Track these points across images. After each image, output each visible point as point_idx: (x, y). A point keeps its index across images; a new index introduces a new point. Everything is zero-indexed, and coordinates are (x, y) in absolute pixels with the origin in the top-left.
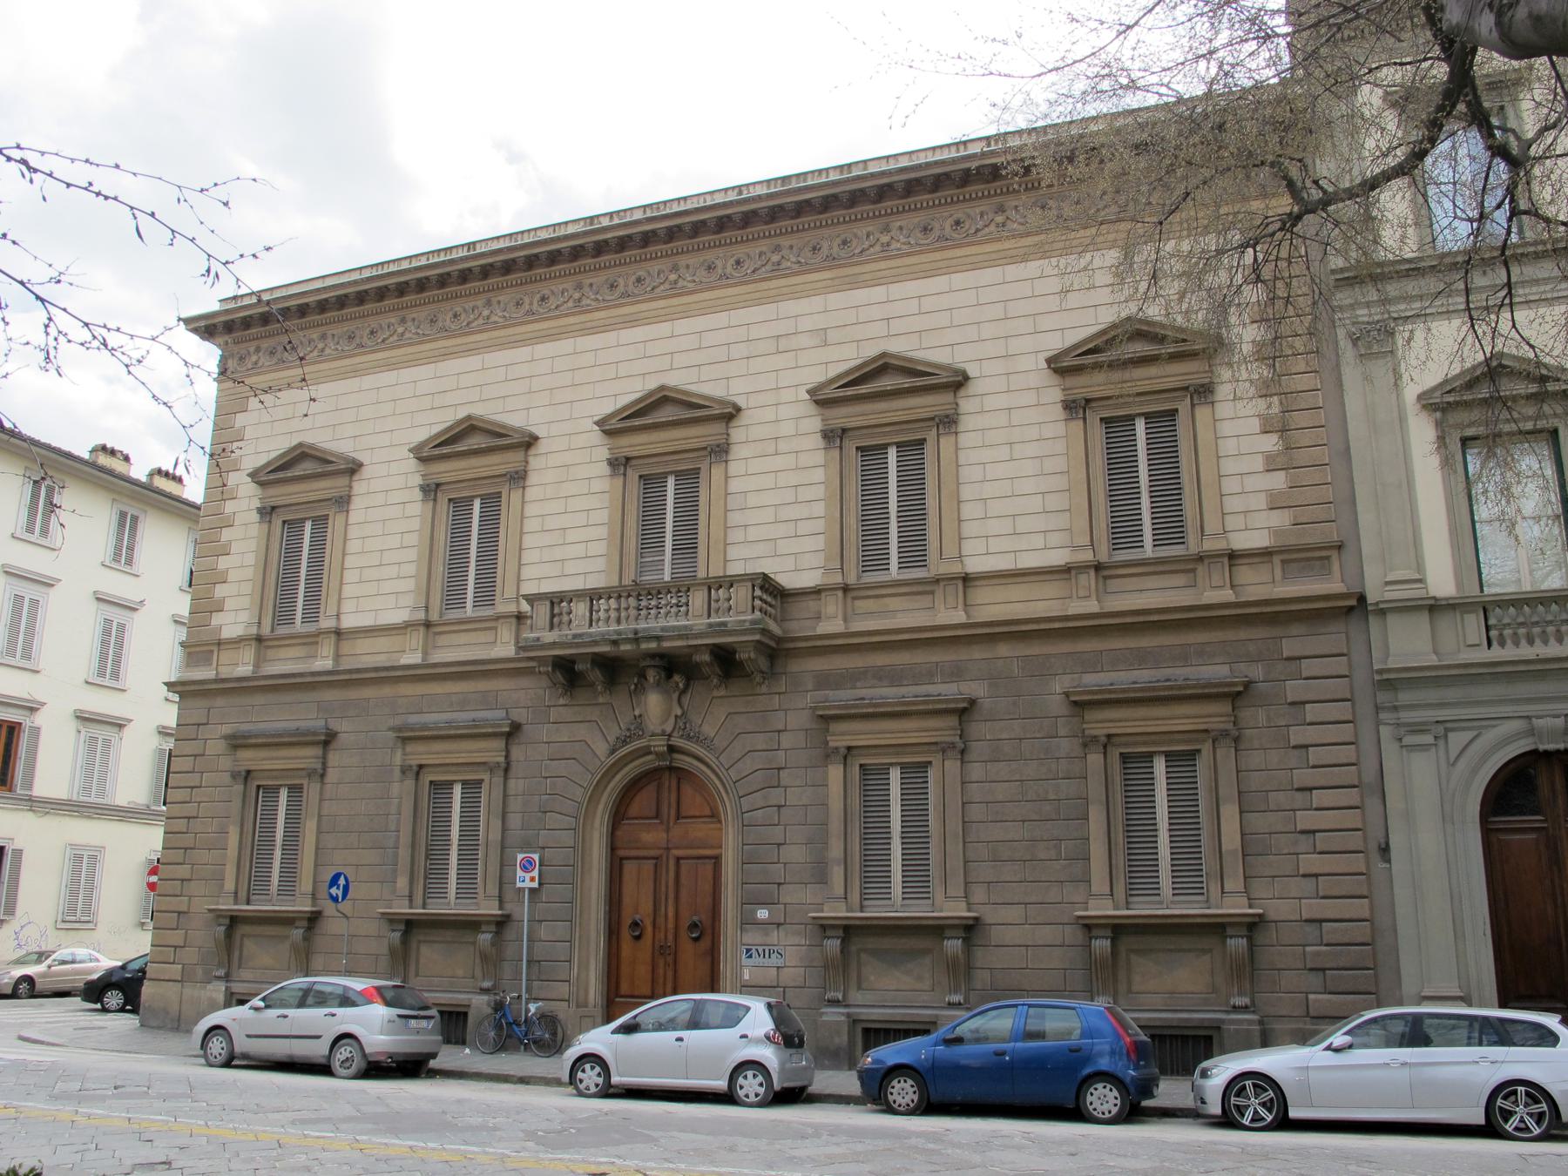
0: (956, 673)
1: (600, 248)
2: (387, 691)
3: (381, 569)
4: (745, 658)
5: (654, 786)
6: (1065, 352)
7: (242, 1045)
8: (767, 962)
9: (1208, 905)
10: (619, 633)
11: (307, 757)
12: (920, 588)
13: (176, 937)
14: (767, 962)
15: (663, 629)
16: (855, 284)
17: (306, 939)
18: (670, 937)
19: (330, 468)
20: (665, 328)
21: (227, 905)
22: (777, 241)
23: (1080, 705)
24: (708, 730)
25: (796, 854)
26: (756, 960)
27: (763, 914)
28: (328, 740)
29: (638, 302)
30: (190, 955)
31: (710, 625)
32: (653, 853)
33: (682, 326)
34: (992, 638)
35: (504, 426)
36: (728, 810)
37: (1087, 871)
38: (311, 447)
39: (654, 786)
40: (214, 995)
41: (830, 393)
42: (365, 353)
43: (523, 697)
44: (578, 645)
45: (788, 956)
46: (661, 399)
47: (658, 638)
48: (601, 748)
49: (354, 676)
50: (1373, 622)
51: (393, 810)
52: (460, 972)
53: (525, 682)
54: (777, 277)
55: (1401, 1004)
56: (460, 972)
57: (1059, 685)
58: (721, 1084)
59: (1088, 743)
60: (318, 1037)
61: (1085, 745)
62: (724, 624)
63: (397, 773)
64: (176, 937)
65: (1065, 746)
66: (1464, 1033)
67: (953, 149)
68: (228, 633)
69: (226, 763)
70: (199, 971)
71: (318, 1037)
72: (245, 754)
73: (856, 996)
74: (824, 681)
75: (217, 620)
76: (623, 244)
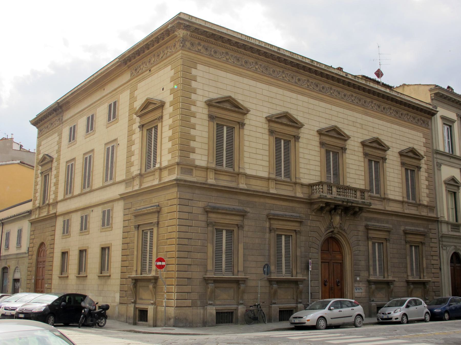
0: (387, 222)
1: (310, 70)
2: (262, 200)
3: (255, 155)
4: (349, 210)
5: (332, 243)
6: (273, 115)
7: (330, 322)
8: (360, 291)
9: (420, 278)
10: (344, 199)
11: (236, 220)
12: (233, 175)
13: (188, 289)
14: (360, 291)
15: (353, 200)
16: (367, 114)
17: (155, 287)
18: (333, 285)
19: (241, 111)
20: (329, 106)
21: (134, 275)
22: (353, 94)
23: (406, 233)
24: (346, 228)
25: (363, 263)
26: (358, 291)
27: (358, 279)
28: (243, 214)
29: (323, 95)
30: (195, 296)
31: (362, 202)
32: (327, 261)
33: (334, 108)
34: (392, 215)
35: (297, 120)
36: (347, 250)
37: (407, 270)
38: (234, 99)
39: (332, 243)
40: (211, 311)
41: (367, 143)
42: (382, 114)
43: (301, 210)
44: (335, 200)
45: (361, 290)
46: (286, 116)
47: (352, 203)
48: (323, 229)
49: (255, 193)
50: (439, 224)
51: (267, 243)
52: (289, 297)
53: (302, 206)
54: (282, 81)
55: (344, 298)
56: (289, 297)
57: (402, 228)
58: (423, 318)
59: (406, 242)
60: (351, 316)
61: (208, 225)
62: (364, 202)
63: (268, 230)
64: (188, 289)
65: (403, 242)
66: (31, 315)
67: (258, 42)
68: (197, 163)
69: (203, 218)
70: (199, 302)
71: (351, 316)
72: (212, 215)
73: (218, 302)
74: (367, 219)
75: (192, 156)
76: (316, 72)
